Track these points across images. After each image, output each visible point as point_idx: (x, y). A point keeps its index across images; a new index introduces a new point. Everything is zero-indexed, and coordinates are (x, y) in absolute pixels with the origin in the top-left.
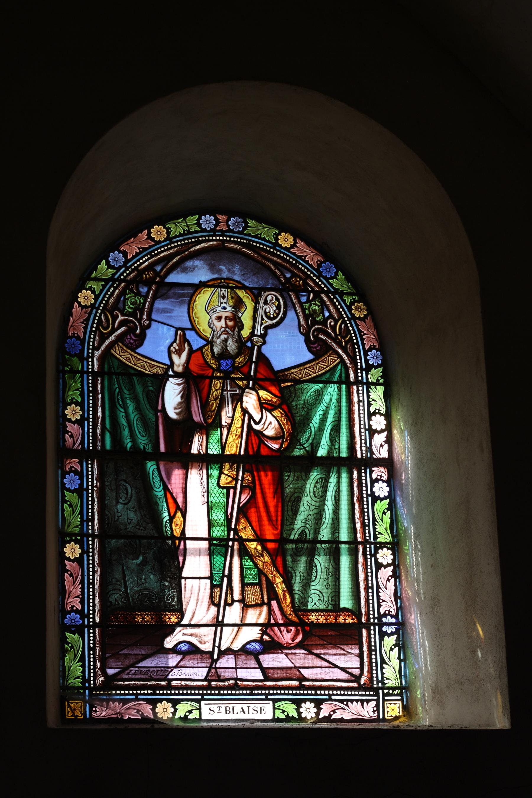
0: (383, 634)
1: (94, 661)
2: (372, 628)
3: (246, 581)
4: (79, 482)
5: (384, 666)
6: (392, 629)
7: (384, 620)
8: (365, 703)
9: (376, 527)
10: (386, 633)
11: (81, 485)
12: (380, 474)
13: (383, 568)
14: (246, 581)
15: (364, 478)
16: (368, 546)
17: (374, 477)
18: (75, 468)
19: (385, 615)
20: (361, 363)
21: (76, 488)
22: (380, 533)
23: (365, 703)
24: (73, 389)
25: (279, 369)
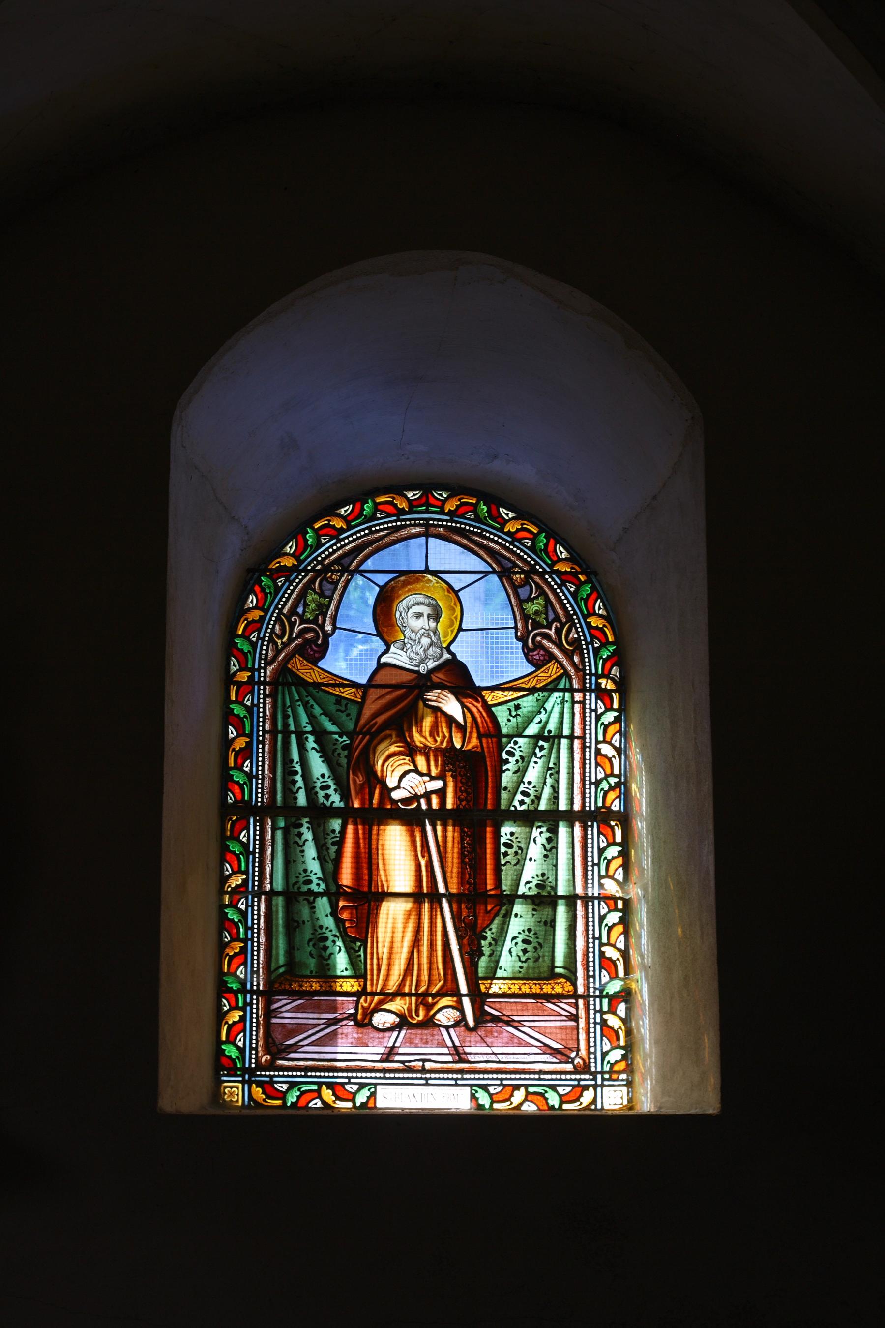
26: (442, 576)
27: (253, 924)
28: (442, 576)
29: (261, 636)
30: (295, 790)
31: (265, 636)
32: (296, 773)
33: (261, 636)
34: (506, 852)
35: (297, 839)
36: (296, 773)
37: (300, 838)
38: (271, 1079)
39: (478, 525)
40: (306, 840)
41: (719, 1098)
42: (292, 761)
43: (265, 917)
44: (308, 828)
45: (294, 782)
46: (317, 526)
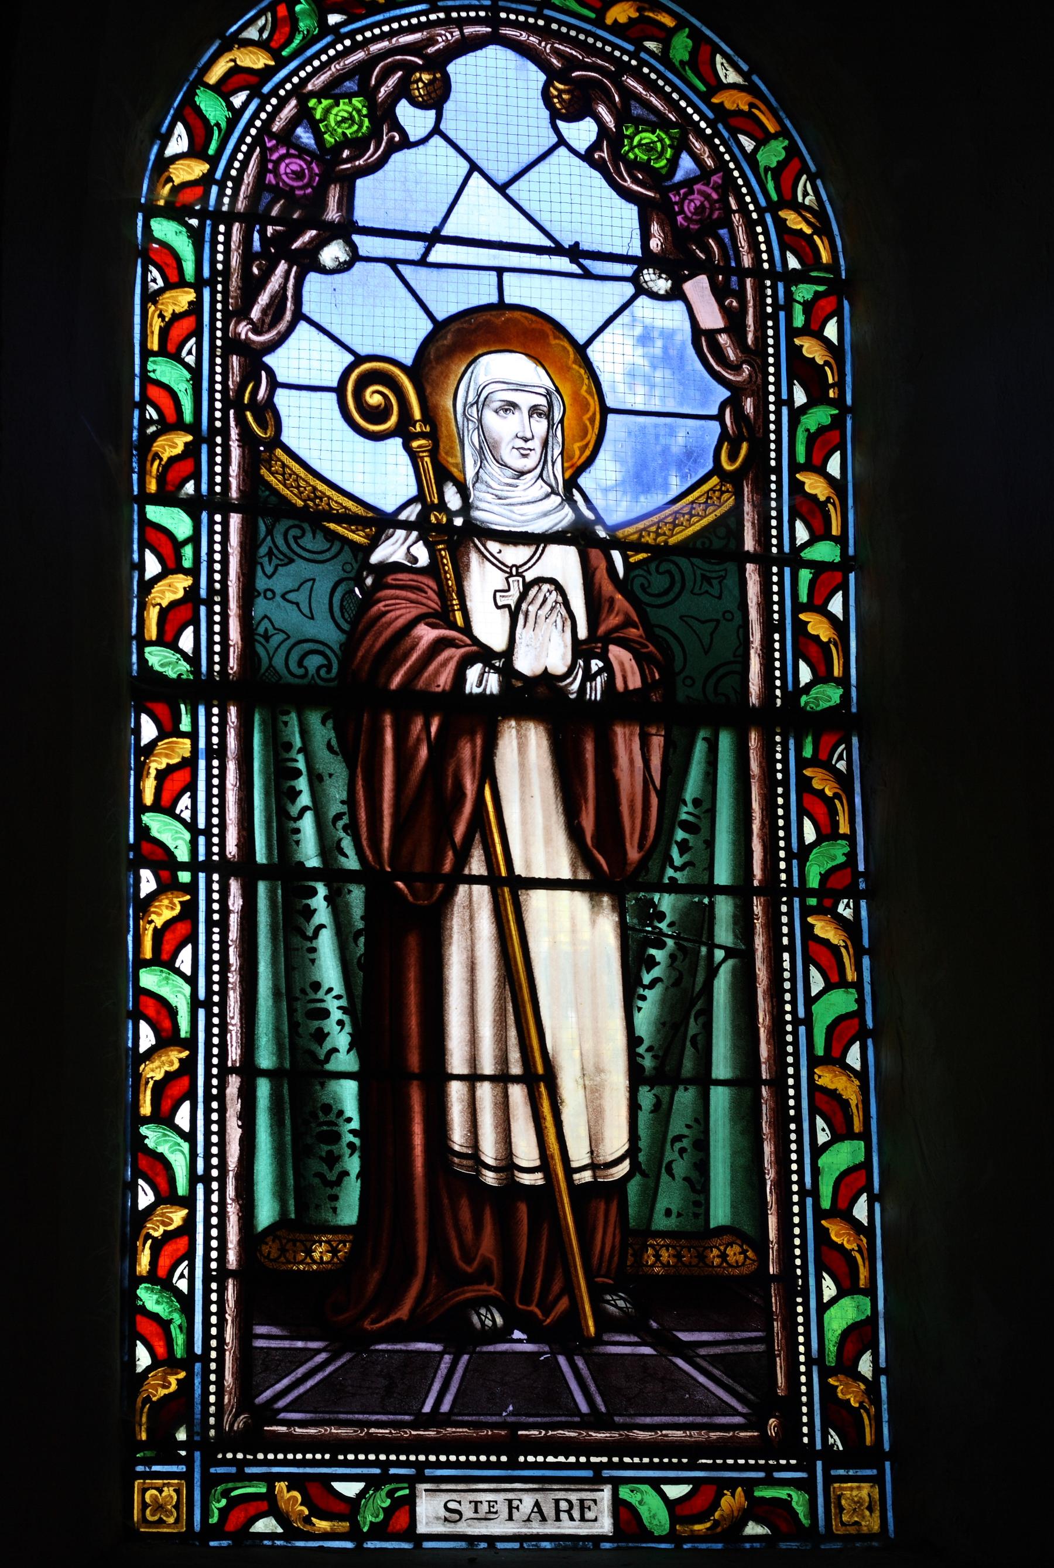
26: (547, 243)
27: (206, 1347)
28: (547, 243)
29: (809, 1201)
30: (310, 933)
31: (802, 1204)
32: (298, 773)
33: (809, 1201)
34: (685, 841)
35: (324, 1169)
36: (298, 773)
37: (321, 1044)
38: (261, 96)
39: (661, 68)
40: (335, 1050)
41: (555, 781)
42: (289, 746)
43: (237, 1177)
44: (341, 1023)
45: (310, 913)
46: (146, 1109)
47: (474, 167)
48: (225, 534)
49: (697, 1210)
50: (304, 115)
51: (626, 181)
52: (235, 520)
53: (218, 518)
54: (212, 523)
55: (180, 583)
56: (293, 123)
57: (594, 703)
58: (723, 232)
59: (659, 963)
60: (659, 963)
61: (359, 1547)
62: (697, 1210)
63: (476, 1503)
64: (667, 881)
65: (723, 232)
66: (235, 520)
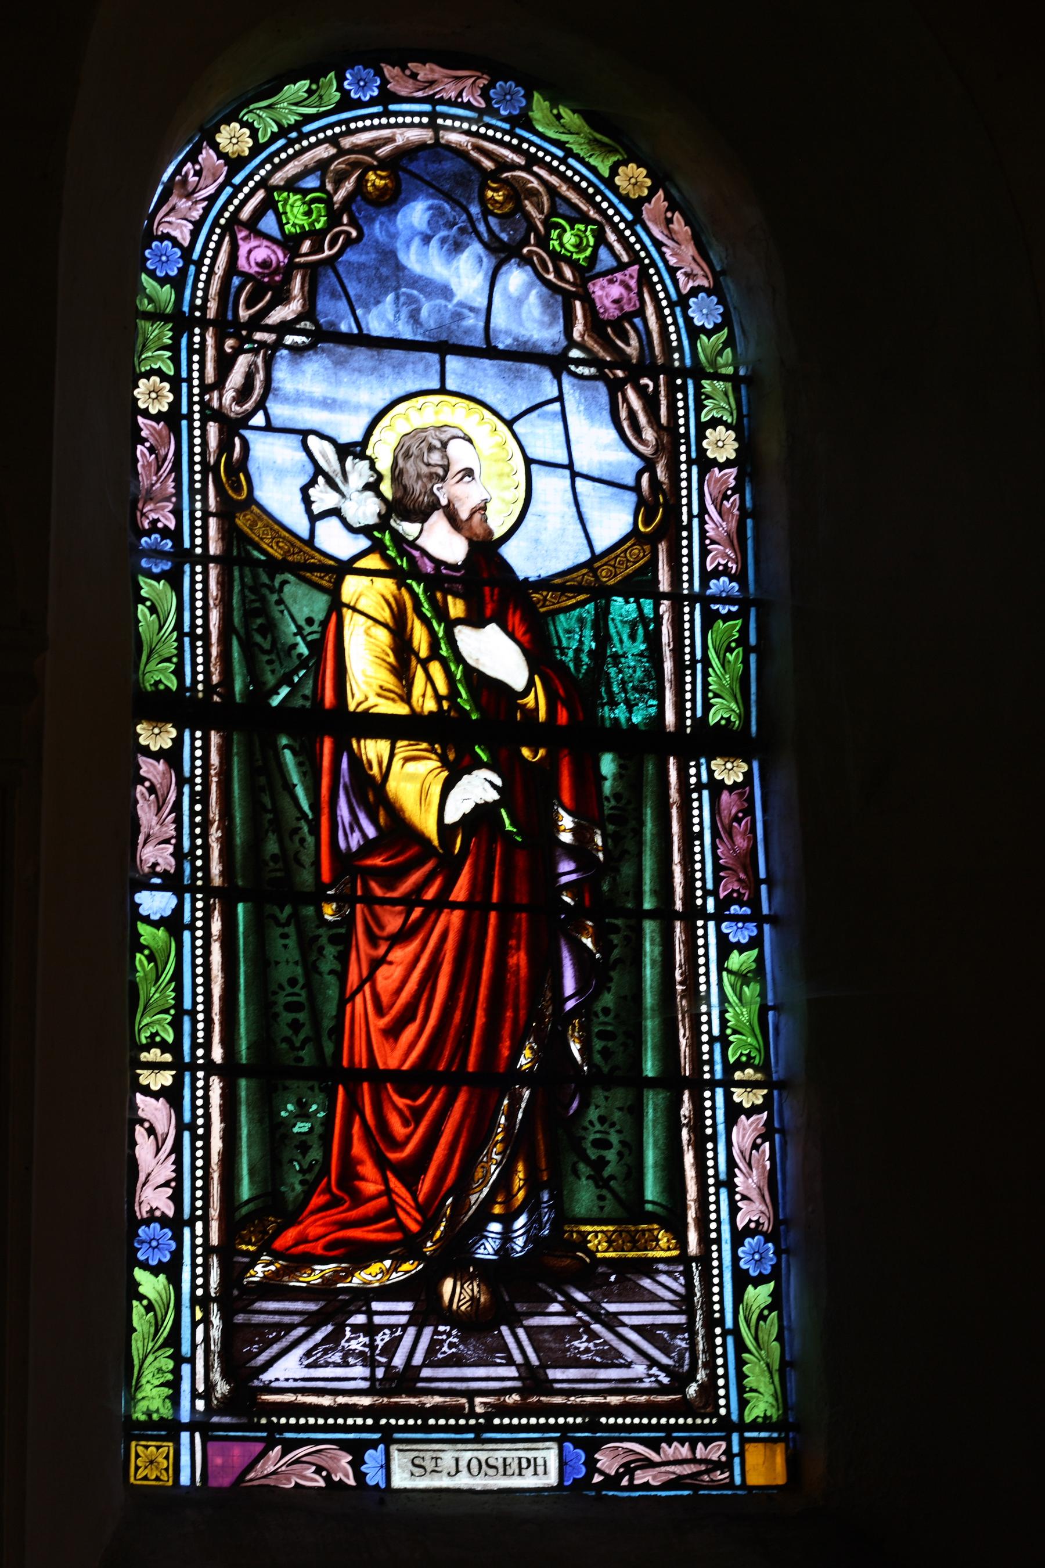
0: (734, 1112)
1: (206, 608)
2: (707, 1094)
3: (435, 385)
4: (173, 1245)
5: (746, 1356)
6: (757, 1097)
7: (738, 1075)
8: (700, 1445)
9: (707, 527)
10: (717, 615)
11: (175, 405)
12: (726, 716)
13: (743, 1117)
14: (435, 385)
15: (687, 617)
16: (700, 923)
17: (704, 418)
18: (166, 686)
19: (716, 574)
20: (691, 581)
21: (170, 1234)
22: (744, 1198)
23: (700, 1445)
24: (158, 660)
25: (505, 556)
47: (443, 390)
48: (205, 582)
49: (602, 1204)
50: (268, 204)
51: (548, 272)
52: (213, 572)
53: (199, 568)
54: (193, 573)
55: (173, 625)
56: (259, 213)
57: (644, 1208)
58: (637, 321)
59: (303, 1025)
60: (303, 1025)
61: (678, 916)
62: (602, 1204)
63: (437, 1459)
64: (542, 752)
65: (637, 321)
66: (213, 572)
